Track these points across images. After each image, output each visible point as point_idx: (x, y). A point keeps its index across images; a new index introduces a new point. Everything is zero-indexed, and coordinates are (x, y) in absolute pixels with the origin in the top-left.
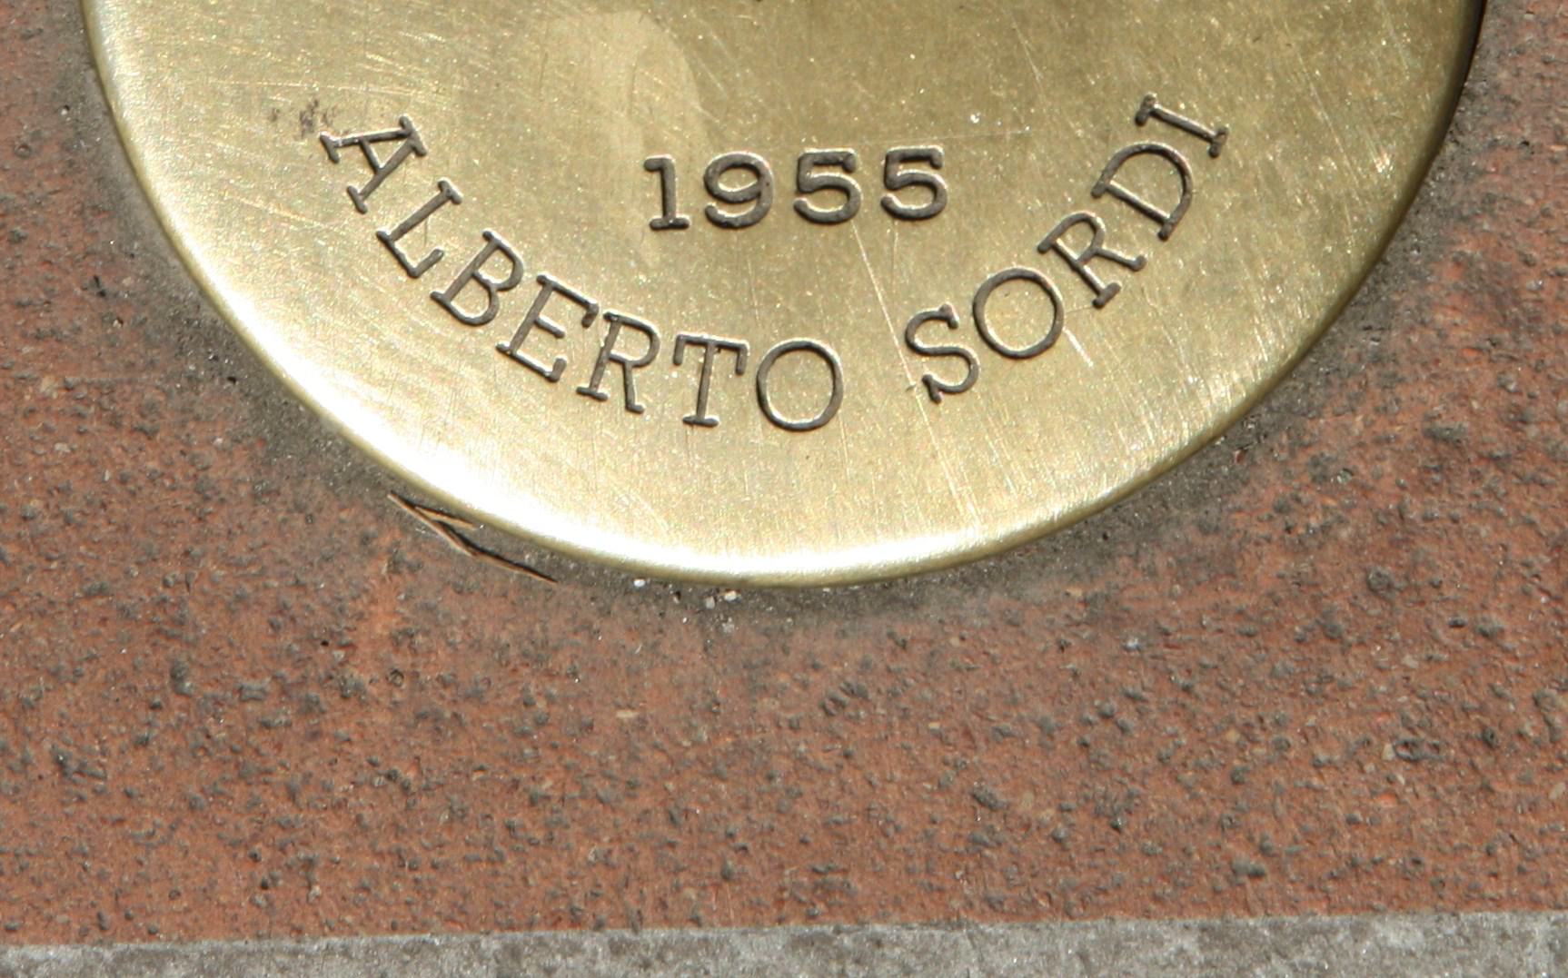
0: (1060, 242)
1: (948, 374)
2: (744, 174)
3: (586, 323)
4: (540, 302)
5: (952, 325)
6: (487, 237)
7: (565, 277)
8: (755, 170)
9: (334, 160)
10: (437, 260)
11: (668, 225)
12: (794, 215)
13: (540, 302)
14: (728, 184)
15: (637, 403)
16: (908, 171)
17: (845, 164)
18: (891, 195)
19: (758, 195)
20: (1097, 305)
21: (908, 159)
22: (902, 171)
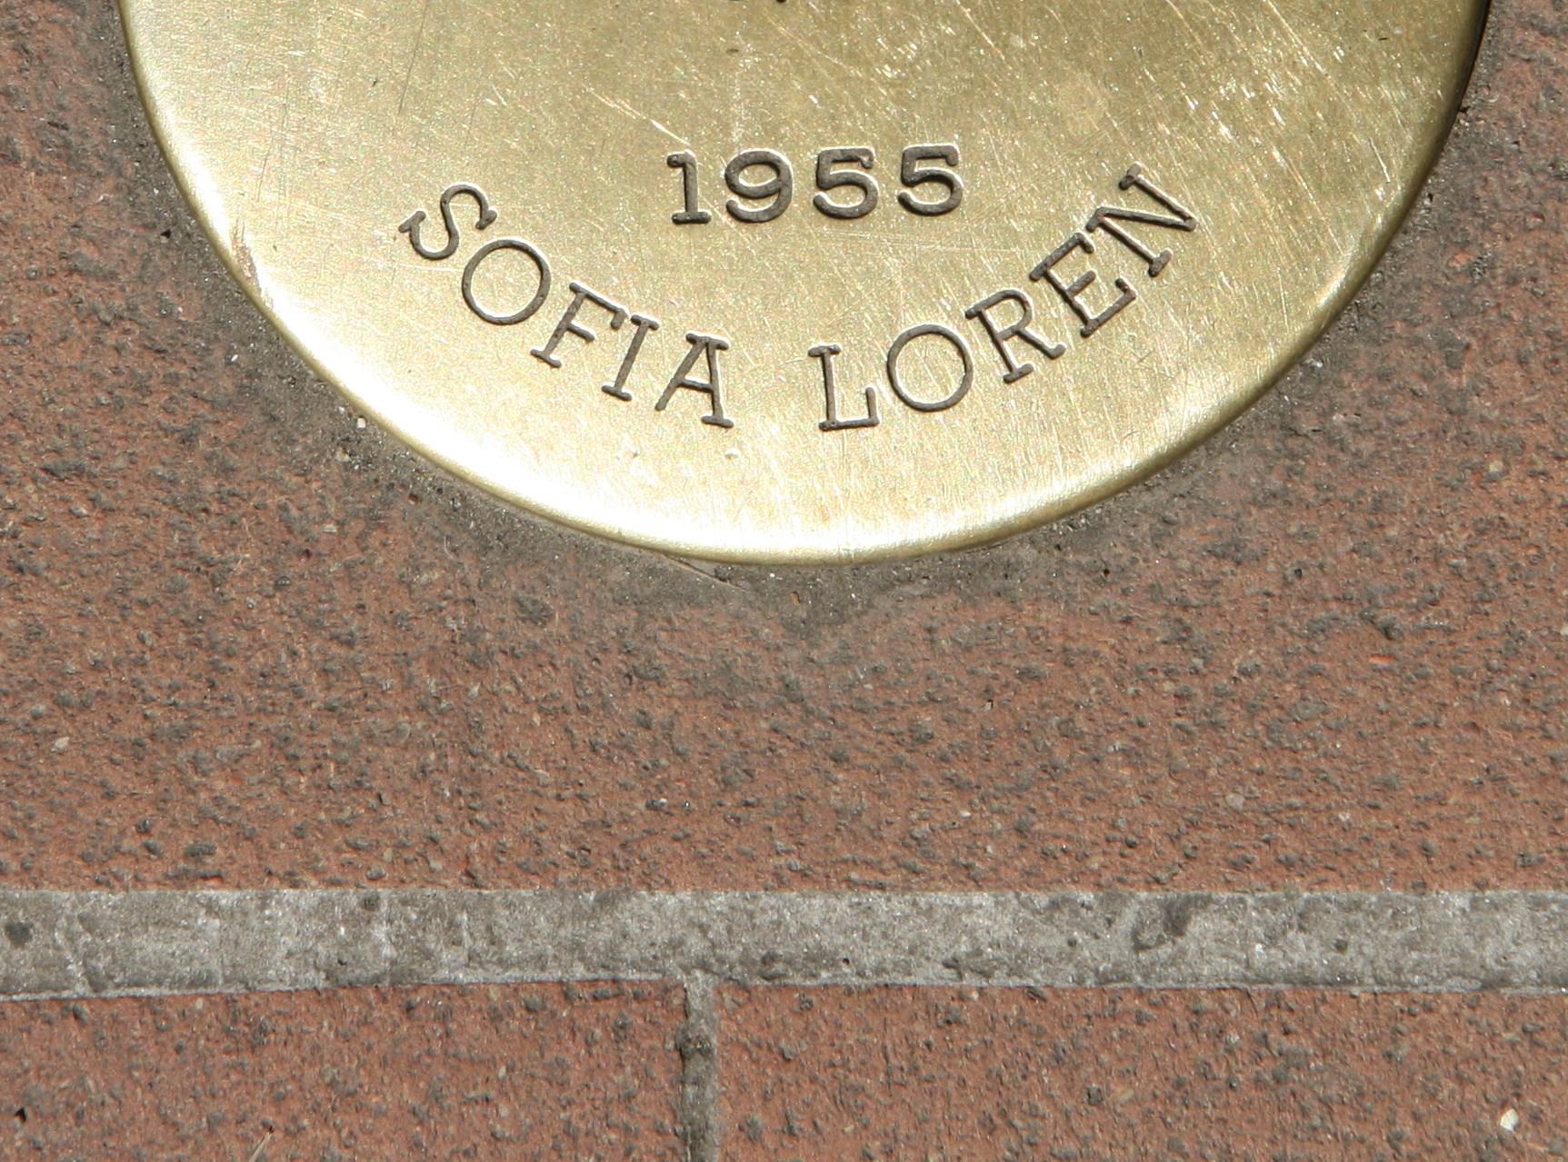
0: (1052, 272)
1: (433, 239)
2: (761, 169)
3: (614, 327)
4: (575, 306)
5: (481, 227)
6: (574, 289)
7: (598, 289)
8: (774, 165)
9: (555, 365)
10: (658, 408)
11: (692, 219)
12: (814, 213)
13: (575, 306)
14: (746, 178)
15: (726, 416)
16: (929, 178)
17: (947, 157)
18: (822, 194)
19: (779, 191)
20: (1152, 274)
21: (850, 158)
22: (920, 168)
